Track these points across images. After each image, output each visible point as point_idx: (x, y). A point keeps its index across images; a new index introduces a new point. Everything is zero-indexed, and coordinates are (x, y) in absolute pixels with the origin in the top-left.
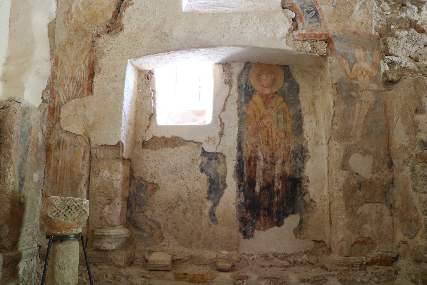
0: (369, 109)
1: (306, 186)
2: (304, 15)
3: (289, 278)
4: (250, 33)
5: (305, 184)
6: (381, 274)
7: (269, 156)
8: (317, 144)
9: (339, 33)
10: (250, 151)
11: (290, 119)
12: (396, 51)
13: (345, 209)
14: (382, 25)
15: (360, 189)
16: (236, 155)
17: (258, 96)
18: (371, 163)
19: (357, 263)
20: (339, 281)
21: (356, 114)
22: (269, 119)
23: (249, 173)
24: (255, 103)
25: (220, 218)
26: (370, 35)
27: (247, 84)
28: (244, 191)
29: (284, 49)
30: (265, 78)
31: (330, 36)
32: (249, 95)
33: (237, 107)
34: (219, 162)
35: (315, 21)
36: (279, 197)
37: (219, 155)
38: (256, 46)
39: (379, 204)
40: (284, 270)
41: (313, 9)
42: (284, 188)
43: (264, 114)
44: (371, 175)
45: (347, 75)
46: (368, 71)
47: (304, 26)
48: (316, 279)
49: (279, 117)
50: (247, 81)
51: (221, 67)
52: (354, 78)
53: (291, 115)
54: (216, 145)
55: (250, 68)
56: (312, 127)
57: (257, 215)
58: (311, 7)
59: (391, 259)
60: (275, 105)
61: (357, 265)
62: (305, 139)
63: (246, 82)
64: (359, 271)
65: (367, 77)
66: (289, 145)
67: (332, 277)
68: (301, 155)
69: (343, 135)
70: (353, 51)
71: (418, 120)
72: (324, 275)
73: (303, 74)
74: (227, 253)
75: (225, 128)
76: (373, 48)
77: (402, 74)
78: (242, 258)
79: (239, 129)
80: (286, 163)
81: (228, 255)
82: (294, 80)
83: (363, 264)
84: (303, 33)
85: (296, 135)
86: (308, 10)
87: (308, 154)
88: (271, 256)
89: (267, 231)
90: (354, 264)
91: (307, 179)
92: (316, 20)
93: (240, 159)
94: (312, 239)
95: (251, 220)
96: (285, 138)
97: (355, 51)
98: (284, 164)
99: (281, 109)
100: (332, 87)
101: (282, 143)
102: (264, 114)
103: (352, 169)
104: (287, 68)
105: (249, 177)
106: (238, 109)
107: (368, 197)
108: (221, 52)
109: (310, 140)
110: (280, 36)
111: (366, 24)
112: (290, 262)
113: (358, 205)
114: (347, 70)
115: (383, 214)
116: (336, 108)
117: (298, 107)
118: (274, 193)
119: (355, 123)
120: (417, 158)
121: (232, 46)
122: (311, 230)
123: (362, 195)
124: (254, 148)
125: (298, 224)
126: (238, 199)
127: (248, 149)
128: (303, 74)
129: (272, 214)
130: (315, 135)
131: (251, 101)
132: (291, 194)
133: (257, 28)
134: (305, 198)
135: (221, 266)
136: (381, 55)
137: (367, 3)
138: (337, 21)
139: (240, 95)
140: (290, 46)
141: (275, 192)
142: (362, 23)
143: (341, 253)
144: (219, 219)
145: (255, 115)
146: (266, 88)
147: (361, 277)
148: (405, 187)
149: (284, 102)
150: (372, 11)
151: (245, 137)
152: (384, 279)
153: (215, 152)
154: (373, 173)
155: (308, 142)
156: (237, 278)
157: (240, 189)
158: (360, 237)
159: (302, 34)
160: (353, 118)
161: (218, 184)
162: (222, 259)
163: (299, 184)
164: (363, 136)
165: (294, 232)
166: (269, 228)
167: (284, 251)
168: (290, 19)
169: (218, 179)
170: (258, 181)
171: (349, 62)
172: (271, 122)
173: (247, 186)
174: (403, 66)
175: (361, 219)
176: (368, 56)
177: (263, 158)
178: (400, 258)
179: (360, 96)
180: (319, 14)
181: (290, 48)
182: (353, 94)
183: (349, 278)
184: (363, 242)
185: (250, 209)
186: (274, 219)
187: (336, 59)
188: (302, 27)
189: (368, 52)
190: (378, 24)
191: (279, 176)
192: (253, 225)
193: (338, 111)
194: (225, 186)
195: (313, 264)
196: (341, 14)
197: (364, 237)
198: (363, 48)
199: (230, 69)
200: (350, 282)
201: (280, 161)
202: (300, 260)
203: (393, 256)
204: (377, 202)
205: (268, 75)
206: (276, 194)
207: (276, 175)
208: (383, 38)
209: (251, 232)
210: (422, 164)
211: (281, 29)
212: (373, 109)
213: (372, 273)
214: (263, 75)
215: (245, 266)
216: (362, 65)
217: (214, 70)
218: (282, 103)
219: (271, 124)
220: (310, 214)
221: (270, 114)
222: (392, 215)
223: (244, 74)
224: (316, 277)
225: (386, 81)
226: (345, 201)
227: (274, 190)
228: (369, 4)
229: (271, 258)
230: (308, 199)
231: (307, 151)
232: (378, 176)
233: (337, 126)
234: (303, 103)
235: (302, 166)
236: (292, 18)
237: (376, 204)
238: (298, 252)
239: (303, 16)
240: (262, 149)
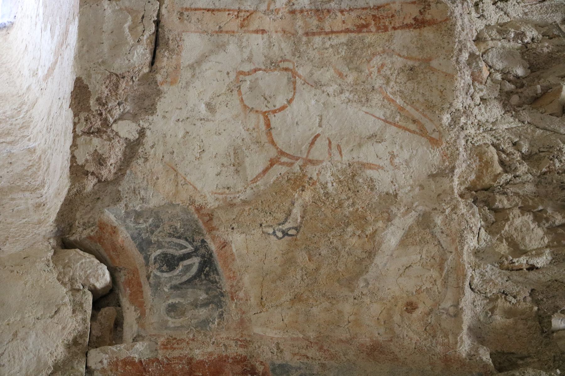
2: (148, 277)
9: (304, 352)
14: (509, 313)
26: (447, 361)
35: (196, 300)
41: (190, 248)
47: (142, 326)
58: (183, 242)
84: (136, 357)
86: (171, 251)
111: (431, 310)
137: (439, 220)
138: (297, 299)
142: (411, 307)
150: (460, 254)
168: (79, 295)
180: (216, 271)
188: (135, 327)
190: (492, 310)
196: (317, 269)
211: (31, 340)
228: (448, 221)
236: (94, 291)
239: (143, 279)
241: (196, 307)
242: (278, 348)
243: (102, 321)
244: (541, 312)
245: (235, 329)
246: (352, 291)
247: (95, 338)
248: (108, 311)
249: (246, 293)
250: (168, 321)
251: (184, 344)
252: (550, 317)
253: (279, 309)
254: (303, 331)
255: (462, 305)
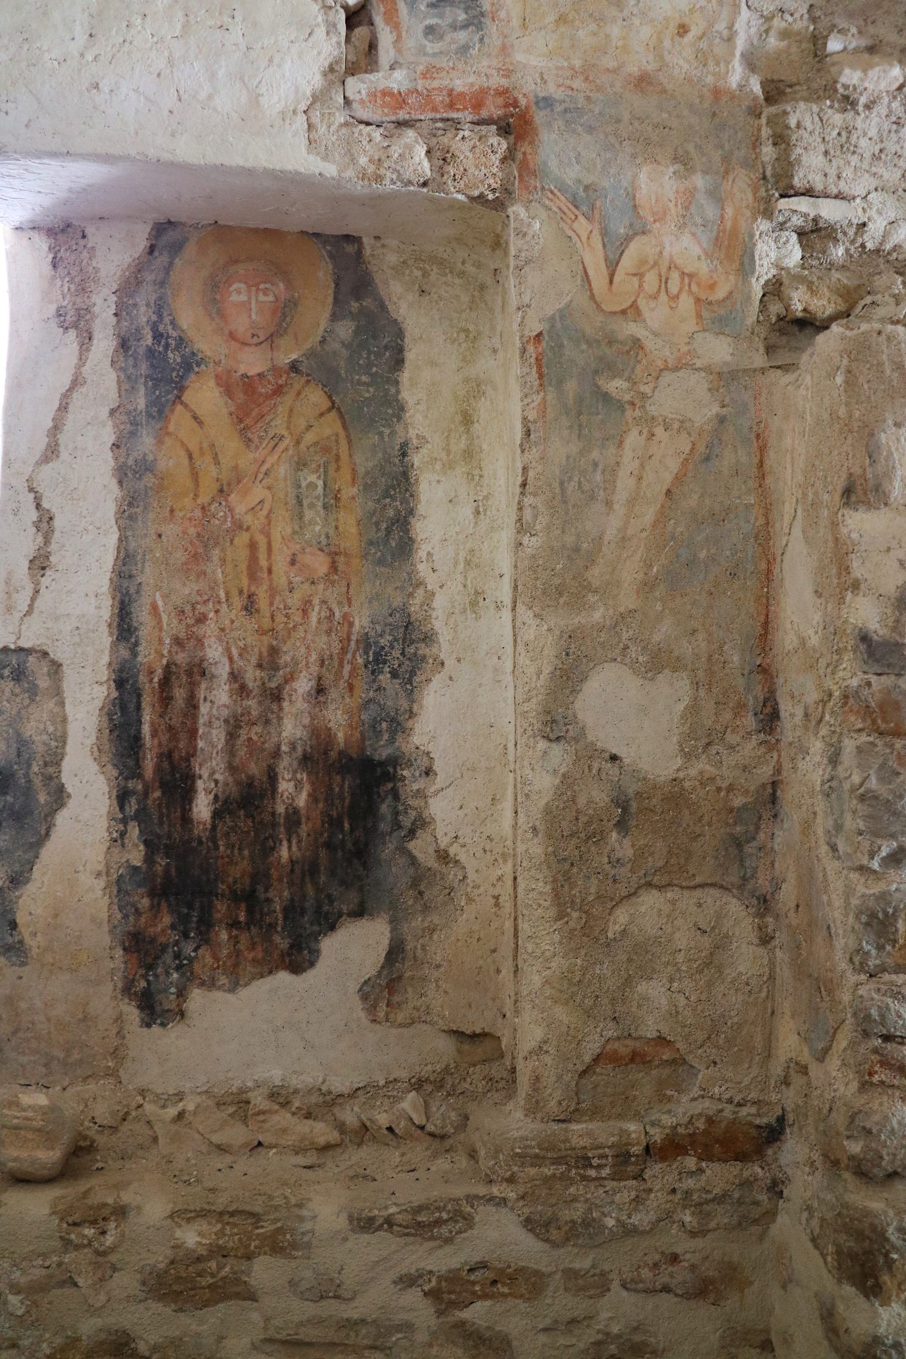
0: (686, 460)
1: (421, 794)
3: (305, 1213)
4: (136, 91)
5: (415, 787)
6: (710, 1196)
7: (254, 660)
8: (474, 604)
9: (568, 82)
10: (168, 641)
11: (354, 491)
12: (832, 172)
13: (552, 913)
14: (785, 34)
15: (622, 825)
16: (106, 659)
17: (212, 383)
18: (681, 706)
19: (601, 1151)
20: (525, 1226)
21: (625, 484)
22: (259, 492)
23: (164, 738)
24: (195, 418)
25: (39, 938)
26: (717, 93)
27: (161, 328)
28: (141, 816)
29: (298, 173)
30: (243, 298)
31: (523, 102)
32: (173, 382)
33: (112, 439)
34: (33, 691)
35: (455, 21)
36: (299, 842)
37: (31, 658)
38: (166, 156)
39: (712, 891)
40: (309, 1167)
42: (321, 805)
43: (236, 468)
44: (679, 761)
45: (592, 297)
46: (691, 276)
47: (399, 51)
48: (420, 1219)
49: (304, 484)
50: (160, 316)
51: (42, 243)
52: (624, 312)
53: (361, 470)
54: (17, 615)
55: (176, 248)
56: (457, 529)
57: (201, 921)
59: (753, 1132)
60: (288, 428)
61: (601, 1157)
62: (420, 584)
63: (154, 318)
64: (615, 1183)
65: (686, 303)
66: (346, 609)
67: (494, 1210)
68: (403, 654)
69: (557, 581)
70: (630, 174)
71: (854, 536)
72: (457, 1200)
73: (426, 274)
74: (41, 1099)
75: (57, 535)
76: (726, 159)
77: (859, 286)
78: (134, 1114)
79: (120, 540)
80: (333, 694)
81: (44, 1112)
82: (383, 307)
83: (628, 1155)
84: (395, 87)
85: (381, 562)
87: (435, 650)
88: (259, 1100)
89: (244, 993)
90: (590, 1155)
91: (424, 762)
92: (462, 16)
93: (124, 675)
94: (446, 1028)
95: (176, 943)
96: (328, 579)
97: (635, 176)
98: (321, 699)
99: (316, 443)
100: (524, 351)
101: (316, 601)
102: (236, 468)
103: (590, 738)
104: (350, 249)
105: (167, 756)
106: (116, 446)
107: (661, 863)
108: (16, 183)
109: (441, 587)
110: (279, 107)
111: (704, 34)
112: (341, 1127)
113: (612, 899)
114: (591, 273)
115: (726, 936)
116: (534, 453)
117: (393, 433)
118: (274, 825)
119: (613, 526)
120: (846, 708)
121: (54, 155)
122: (438, 986)
123: (630, 852)
124: (188, 626)
125: (382, 959)
126: (116, 851)
127: (161, 630)
128: (426, 274)
129: (268, 920)
130: (468, 563)
131: (179, 408)
132: (352, 830)
133: (170, 62)
134: (414, 846)
135: (15, 1160)
136: (762, 193)
139: (127, 384)
140: (325, 158)
141: (282, 821)
142: (683, 29)
143: (534, 1108)
144: (33, 943)
145: (195, 476)
146: (247, 349)
147: (621, 1209)
148: (807, 827)
149: (329, 410)
151: (148, 575)
152: (722, 1216)
153: (12, 647)
154: (688, 756)
155: (433, 594)
156: (76, 1217)
157: (127, 808)
158: (618, 1038)
159: (386, 93)
160: (609, 504)
161: (28, 791)
162: (17, 1128)
163: (390, 785)
164: (647, 586)
165: (365, 997)
166: (255, 977)
167: (321, 1080)
168: (332, 13)
169: (29, 766)
170: (205, 773)
171: (604, 233)
172: (267, 506)
173: (157, 794)
174: (870, 246)
175: (624, 957)
176: (701, 197)
177: (227, 669)
178: (788, 1131)
179: (644, 396)
181: (326, 164)
182: (616, 386)
183: (566, 1214)
184: (632, 1060)
185: (172, 899)
186: (277, 939)
187: (544, 214)
188: (392, 52)
189: (699, 181)
190: (767, 31)
191: (300, 749)
192: (184, 966)
193: (540, 468)
194: (60, 796)
195: (443, 1137)
197: (635, 1039)
198: (676, 159)
199: (85, 254)
200: (571, 1229)
201: (303, 685)
202: (383, 1119)
203: (764, 1121)
204: (702, 886)
205: (257, 285)
206: (282, 829)
207: (284, 748)
208: (774, 109)
209: (172, 997)
210: (864, 738)
211: (287, 65)
212: (707, 459)
213: (674, 1191)
214: (235, 286)
215: (141, 1147)
216: (667, 245)
217: (13, 258)
218: (322, 415)
219: (268, 516)
220: (435, 919)
221: (264, 469)
222: (765, 940)
223: (149, 277)
224: (420, 1209)
225: (780, 319)
226: (555, 881)
227: (273, 814)
229: (263, 1112)
230: (431, 850)
231: (428, 638)
232: (708, 767)
233: (533, 539)
234: (419, 417)
235: (404, 704)
236: (346, 8)
237: (698, 893)
238: (382, 1083)
240: (222, 630)
241: (455, 29)
242: (542, 79)
243: (357, 44)
244: (817, 32)
245: (497, 56)
246: (622, 11)
247: (350, 65)
248: (361, 31)
249: (508, 12)
250: (425, 46)
251: (444, 74)
252: (826, 37)
253: (543, 32)
254: (568, 59)
255: (737, 26)
